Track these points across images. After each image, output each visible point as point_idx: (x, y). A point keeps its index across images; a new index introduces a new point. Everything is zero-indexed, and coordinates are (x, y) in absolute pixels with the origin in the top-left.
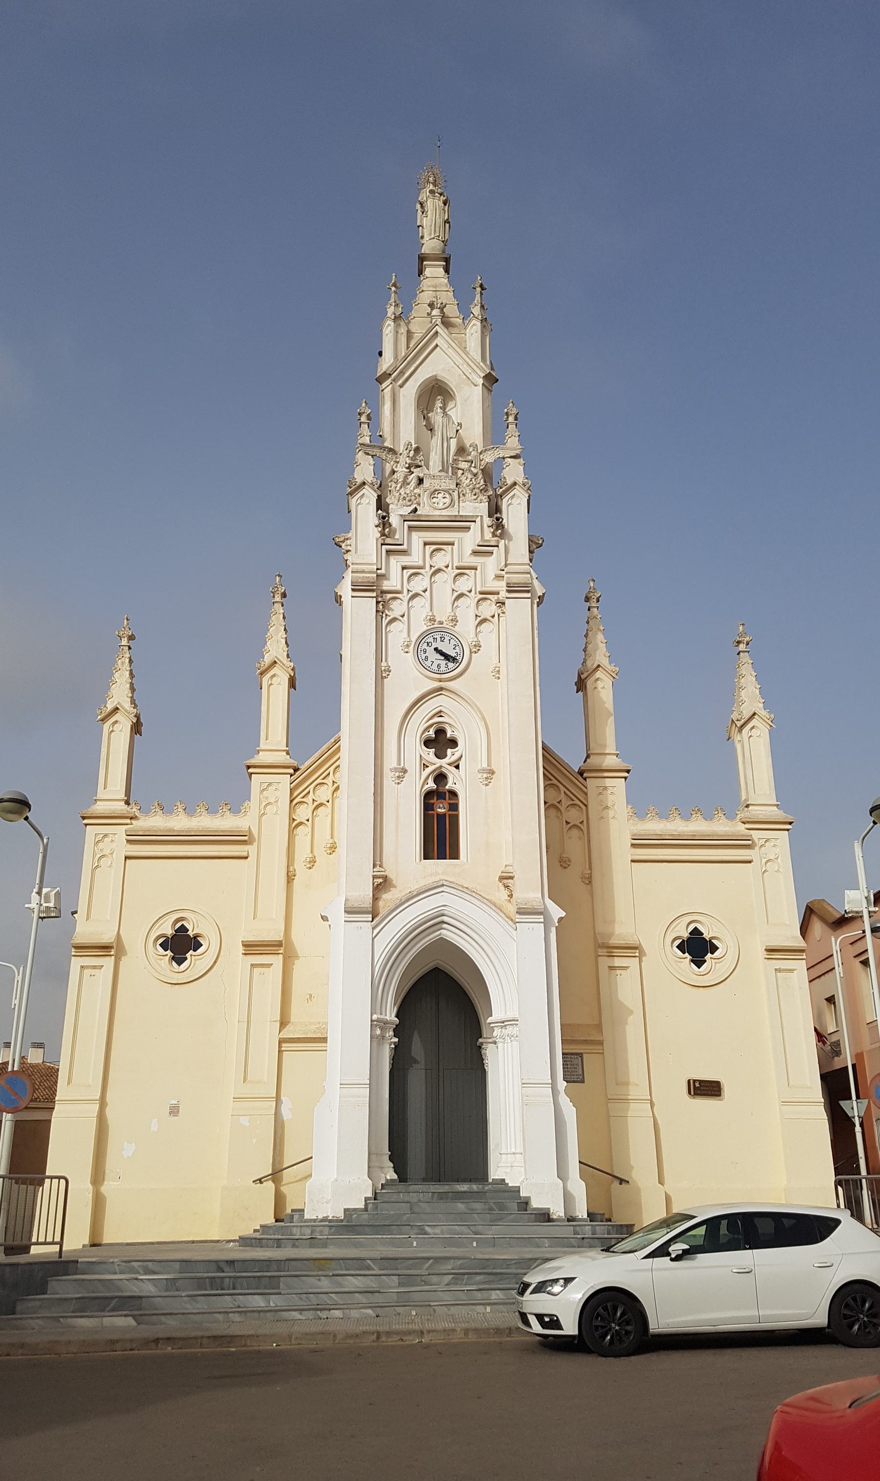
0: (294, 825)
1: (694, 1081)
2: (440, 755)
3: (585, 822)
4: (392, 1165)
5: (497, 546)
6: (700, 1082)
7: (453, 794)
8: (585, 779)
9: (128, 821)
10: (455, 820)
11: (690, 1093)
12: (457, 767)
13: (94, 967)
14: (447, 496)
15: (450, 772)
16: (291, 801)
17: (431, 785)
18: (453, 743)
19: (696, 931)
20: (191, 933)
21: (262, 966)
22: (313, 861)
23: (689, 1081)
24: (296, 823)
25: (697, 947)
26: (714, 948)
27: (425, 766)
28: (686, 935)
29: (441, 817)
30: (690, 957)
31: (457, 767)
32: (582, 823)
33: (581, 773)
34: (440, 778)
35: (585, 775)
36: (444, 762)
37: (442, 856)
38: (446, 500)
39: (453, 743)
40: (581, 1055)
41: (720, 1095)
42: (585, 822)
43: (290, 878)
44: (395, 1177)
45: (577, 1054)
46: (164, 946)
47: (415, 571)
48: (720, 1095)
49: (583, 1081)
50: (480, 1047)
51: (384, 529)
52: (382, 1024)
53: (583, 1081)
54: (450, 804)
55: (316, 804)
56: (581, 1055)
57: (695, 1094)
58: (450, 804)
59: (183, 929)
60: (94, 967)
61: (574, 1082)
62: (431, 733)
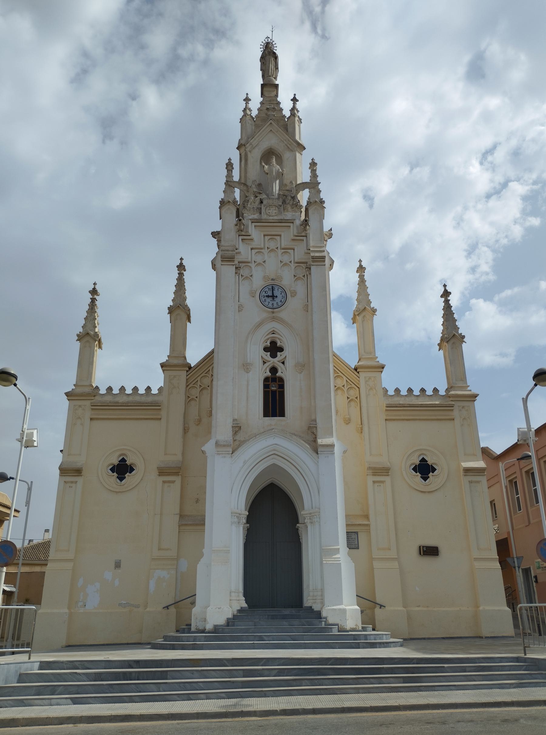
0: (189, 400)
1: (423, 547)
2: (274, 356)
3: (358, 398)
4: (244, 599)
5: (306, 236)
6: (427, 547)
7: (281, 380)
8: (358, 373)
9: (93, 398)
10: (282, 394)
11: (420, 554)
12: (283, 363)
13: (72, 482)
14: (277, 209)
15: (280, 366)
16: (187, 386)
17: (269, 374)
18: (281, 349)
19: (423, 460)
20: (128, 463)
21: (169, 482)
22: (200, 421)
23: (420, 547)
24: (190, 399)
25: (424, 469)
26: (434, 470)
27: (264, 363)
28: (418, 462)
29: (274, 392)
30: (420, 475)
31: (283, 363)
32: (357, 398)
33: (356, 369)
34: (274, 370)
35: (358, 370)
36: (275, 360)
37: (274, 415)
38: (275, 211)
39: (281, 349)
40: (357, 533)
41: (438, 555)
42: (358, 398)
43: (186, 430)
44: (246, 605)
45: (355, 532)
46: (112, 470)
47: (259, 250)
48: (438, 555)
49: (358, 548)
50: (298, 529)
51: (240, 226)
52: (239, 515)
53: (358, 548)
54: (279, 385)
55: (201, 388)
56: (357, 533)
57: (424, 554)
58: (279, 385)
59: (123, 460)
60: (72, 482)
61: (353, 548)
62: (268, 344)
